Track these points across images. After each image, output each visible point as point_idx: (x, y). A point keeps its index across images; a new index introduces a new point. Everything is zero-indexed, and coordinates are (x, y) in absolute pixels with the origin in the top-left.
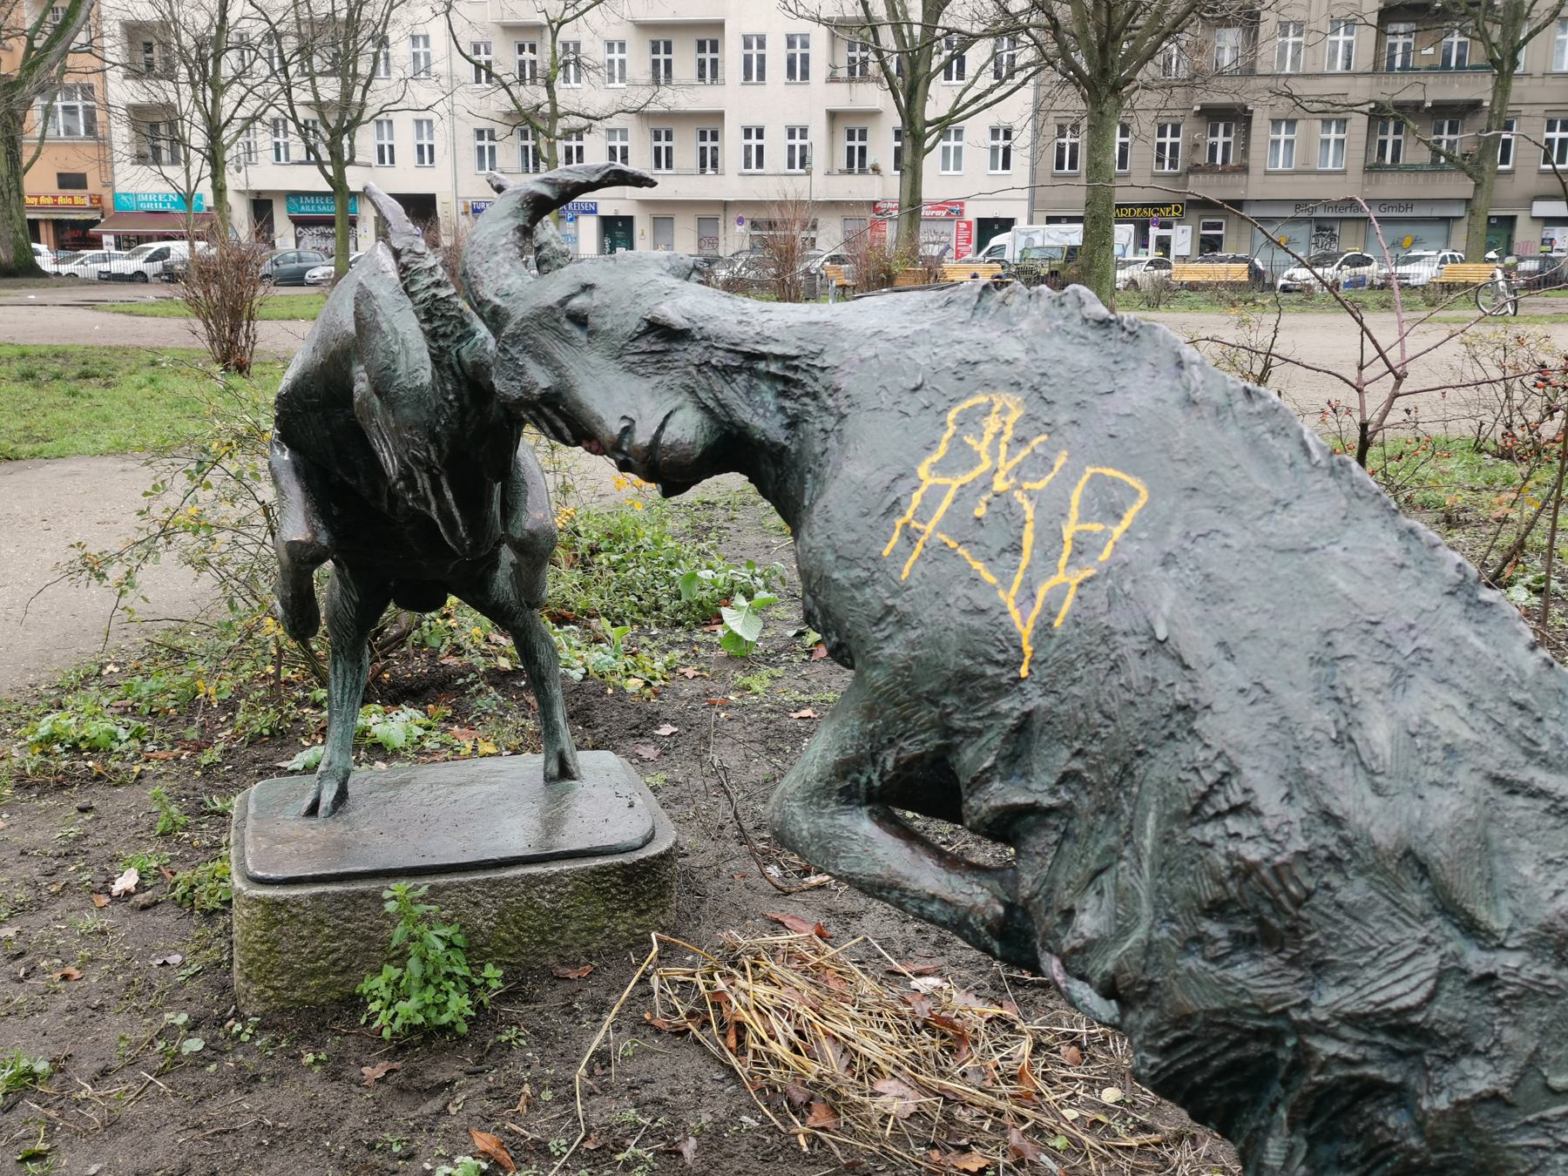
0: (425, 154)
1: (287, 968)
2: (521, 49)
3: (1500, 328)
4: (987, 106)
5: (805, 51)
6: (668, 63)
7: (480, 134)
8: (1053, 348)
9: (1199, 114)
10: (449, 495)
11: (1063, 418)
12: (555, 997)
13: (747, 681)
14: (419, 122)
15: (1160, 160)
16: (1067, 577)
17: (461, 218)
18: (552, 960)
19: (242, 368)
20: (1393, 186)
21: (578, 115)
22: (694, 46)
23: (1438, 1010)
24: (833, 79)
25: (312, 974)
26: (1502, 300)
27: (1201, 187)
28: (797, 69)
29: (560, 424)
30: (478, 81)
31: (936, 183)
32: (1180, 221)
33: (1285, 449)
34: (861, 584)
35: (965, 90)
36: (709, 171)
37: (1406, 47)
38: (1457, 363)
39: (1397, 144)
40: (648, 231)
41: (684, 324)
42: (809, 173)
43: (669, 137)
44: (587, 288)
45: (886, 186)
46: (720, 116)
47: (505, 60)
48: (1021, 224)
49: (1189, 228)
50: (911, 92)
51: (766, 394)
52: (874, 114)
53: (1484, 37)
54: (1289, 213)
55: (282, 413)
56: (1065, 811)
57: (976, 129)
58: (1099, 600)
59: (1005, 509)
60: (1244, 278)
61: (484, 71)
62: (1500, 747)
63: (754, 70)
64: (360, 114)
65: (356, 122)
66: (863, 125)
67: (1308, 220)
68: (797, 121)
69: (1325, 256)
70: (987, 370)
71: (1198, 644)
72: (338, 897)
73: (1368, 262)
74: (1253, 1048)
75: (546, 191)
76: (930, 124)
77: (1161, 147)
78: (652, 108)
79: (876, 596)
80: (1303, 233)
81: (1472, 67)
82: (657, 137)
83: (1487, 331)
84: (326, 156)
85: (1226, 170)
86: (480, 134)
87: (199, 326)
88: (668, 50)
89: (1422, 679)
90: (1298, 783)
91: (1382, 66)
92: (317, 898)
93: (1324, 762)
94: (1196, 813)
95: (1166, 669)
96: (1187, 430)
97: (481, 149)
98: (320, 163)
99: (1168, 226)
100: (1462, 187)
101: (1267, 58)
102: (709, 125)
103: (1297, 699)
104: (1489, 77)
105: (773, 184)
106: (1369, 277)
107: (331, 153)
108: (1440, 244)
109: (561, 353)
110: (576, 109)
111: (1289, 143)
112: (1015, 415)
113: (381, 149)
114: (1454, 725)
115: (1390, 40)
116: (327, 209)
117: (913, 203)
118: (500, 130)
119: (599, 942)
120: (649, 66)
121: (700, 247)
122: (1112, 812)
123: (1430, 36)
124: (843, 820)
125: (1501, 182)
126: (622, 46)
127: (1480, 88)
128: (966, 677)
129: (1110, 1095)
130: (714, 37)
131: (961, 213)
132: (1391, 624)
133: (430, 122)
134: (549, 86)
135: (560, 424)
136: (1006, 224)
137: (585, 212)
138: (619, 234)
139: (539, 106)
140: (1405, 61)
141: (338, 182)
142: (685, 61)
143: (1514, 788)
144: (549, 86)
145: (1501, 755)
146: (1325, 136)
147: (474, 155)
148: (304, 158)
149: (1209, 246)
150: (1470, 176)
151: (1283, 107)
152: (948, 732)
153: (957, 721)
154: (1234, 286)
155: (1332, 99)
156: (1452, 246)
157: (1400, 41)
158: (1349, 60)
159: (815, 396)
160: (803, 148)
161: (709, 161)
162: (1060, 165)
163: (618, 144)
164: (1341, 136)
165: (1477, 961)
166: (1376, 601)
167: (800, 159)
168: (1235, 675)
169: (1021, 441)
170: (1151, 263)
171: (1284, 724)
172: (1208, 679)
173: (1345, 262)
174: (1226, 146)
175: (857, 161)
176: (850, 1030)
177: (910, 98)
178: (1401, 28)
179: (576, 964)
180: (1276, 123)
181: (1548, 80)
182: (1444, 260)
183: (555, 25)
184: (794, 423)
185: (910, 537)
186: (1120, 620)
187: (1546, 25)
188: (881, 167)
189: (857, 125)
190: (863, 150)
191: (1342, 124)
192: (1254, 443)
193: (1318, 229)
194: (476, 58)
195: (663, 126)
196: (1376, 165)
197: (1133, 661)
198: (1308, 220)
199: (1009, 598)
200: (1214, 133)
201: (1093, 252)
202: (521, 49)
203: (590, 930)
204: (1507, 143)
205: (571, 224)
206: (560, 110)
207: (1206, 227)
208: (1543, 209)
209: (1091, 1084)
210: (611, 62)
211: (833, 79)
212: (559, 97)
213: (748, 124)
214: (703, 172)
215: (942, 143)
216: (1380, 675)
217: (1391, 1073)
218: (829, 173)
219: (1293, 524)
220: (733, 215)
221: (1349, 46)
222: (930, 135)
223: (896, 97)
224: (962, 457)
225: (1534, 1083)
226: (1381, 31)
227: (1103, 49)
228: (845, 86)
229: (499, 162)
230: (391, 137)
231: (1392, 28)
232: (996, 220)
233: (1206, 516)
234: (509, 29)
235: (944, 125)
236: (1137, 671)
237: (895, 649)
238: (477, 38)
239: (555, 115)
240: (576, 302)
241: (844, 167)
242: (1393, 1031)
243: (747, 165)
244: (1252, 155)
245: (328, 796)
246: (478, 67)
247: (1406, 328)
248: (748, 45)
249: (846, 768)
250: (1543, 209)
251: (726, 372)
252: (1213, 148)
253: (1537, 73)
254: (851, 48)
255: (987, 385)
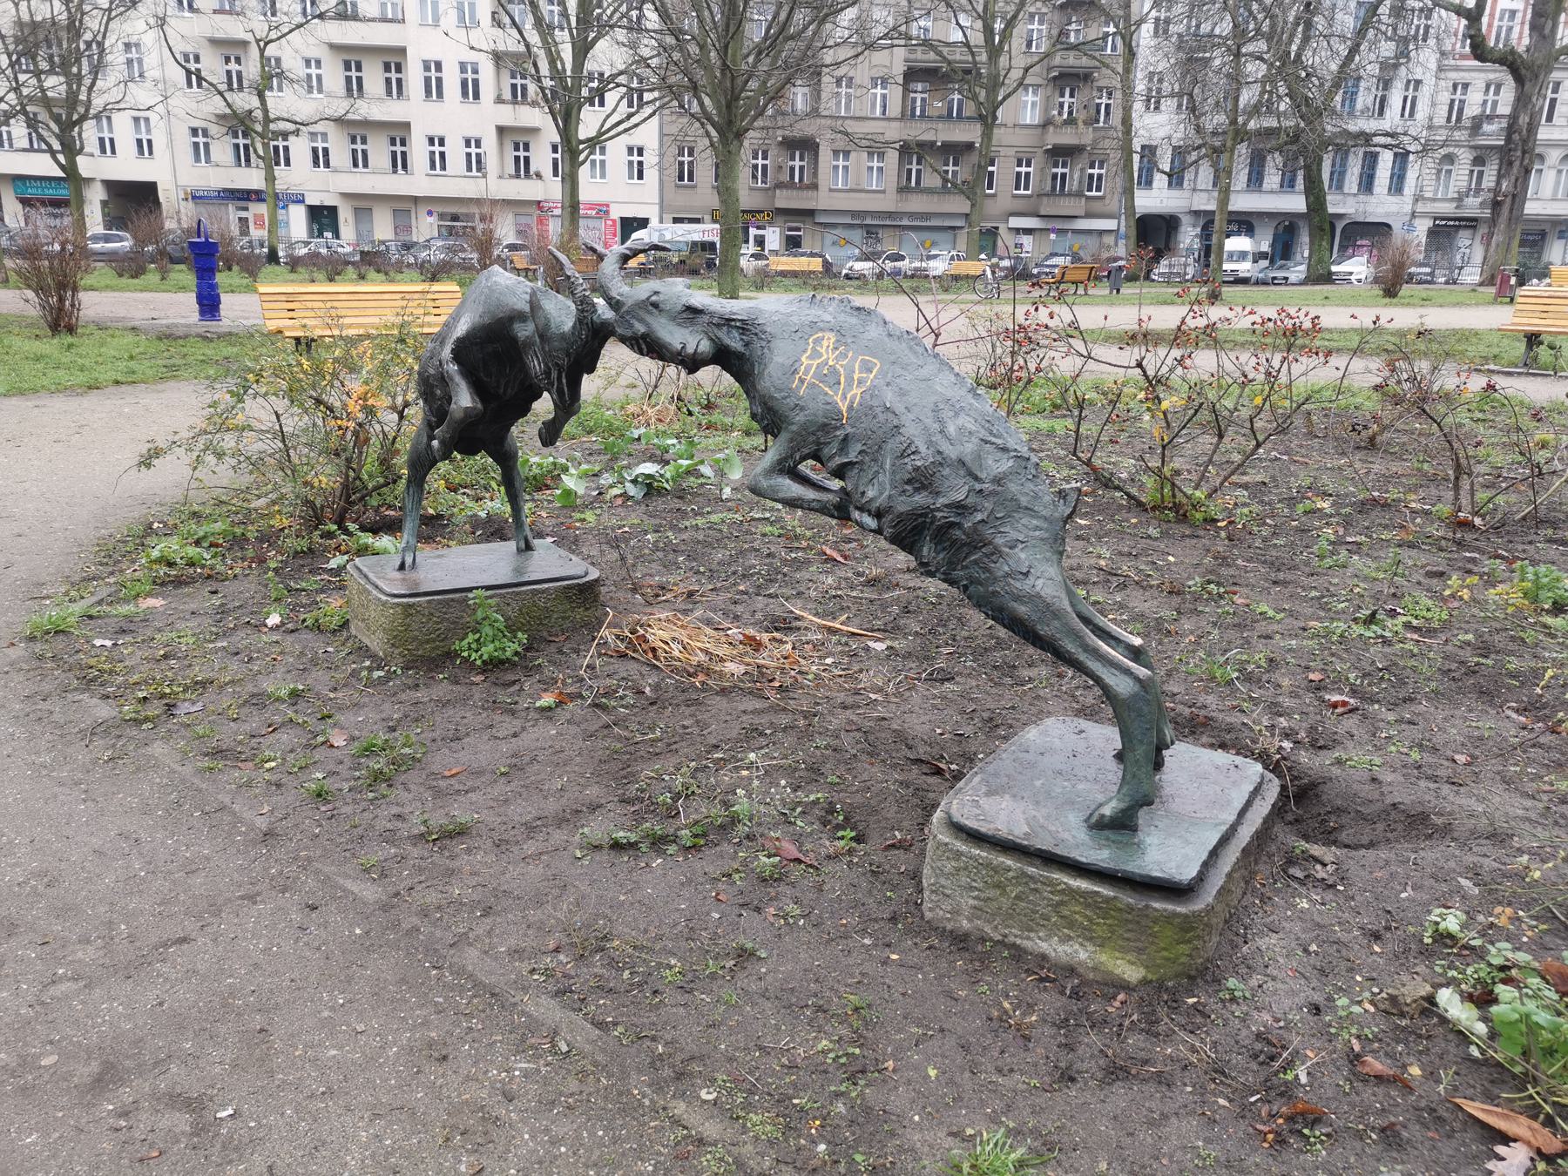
0: (144, 148)
1: (415, 639)
2: (227, 60)
3: (988, 308)
4: (626, 130)
5: (475, 76)
6: (359, 79)
7: (194, 131)
8: (842, 317)
9: (781, 143)
10: (564, 381)
11: (849, 341)
12: (553, 648)
13: (582, 516)
14: (136, 120)
15: (755, 177)
16: (856, 391)
17: (183, 203)
18: (545, 634)
19: (71, 330)
20: (917, 204)
21: (283, 119)
22: (381, 67)
23: (968, 500)
24: (499, 100)
25: (428, 642)
26: (990, 287)
27: (784, 200)
28: (470, 90)
29: (644, 346)
30: (190, 85)
31: (590, 189)
32: (771, 224)
33: (920, 350)
34: (785, 398)
35: (608, 116)
36: (400, 171)
37: (923, 100)
38: (964, 330)
39: (919, 172)
40: (351, 219)
41: (700, 307)
42: (485, 176)
43: (364, 141)
44: (656, 293)
45: (551, 189)
46: (406, 126)
47: (212, 67)
48: (654, 222)
49: (778, 230)
50: (567, 119)
51: (735, 333)
52: (534, 131)
53: (975, 97)
54: (848, 220)
55: (457, 346)
56: (861, 463)
57: (616, 151)
58: (868, 397)
59: (833, 371)
60: (820, 269)
61: (194, 77)
62: (983, 431)
63: (434, 89)
64: (87, 110)
65: (84, 118)
66: (525, 139)
67: (861, 226)
68: (473, 133)
69: (873, 253)
70: (821, 325)
71: (899, 408)
72: (440, 602)
73: (902, 258)
74: (920, 520)
75: (628, 252)
76: (582, 142)
77: (755, 167)
78: (350, 116)
79: (791, 402)
80: (857, 236)
81: (968, 118)
82: (354, 141)
83: (980, 309)
84: (56, 146)
85: (802, 187)
86: (194, 131)
87: (30, 294)
88: (359, 68)
89: (962, 415)
90: (930, 444)
91: (907, 115)
92: (429, 602)
93: (937, 438)
94: (902, 456)
95: (890, 415)
96: (891, 344)
97: (196, 145)
98: (53, 153)
99: (763, 228)
100: (960, 205)
101: (828, 106)
102: (398, 133)
103: (929, 422)
104: (979, 126)
105: (456, 184)
106: (903, 269)
107: (62, 144)
108: (949, 246)
109: (649, 319)
110: (285, 116)
111: (846, 168)
112: (833, 340)
113: (102, 140)
114: (971, 426)
115: (912, 95)
116: (63, 192)
117: (573, 206)
118: (214, 130)
119: (567, 624)
120: (343, 82)
121: (396, 234)
122: (875, 460)
123: (939, 94)
124: (780, 480)
125: (989, 202)
126: (318, 63)
127: (969, 133)
128: (825, 425)
129: (829, 661)
130: (397, 60)
131: (607, 212)
132: (954, 400)
133: (147, 120)
134: (261, 96)
135: (644, 346)
136: (643, 223)
137: (293, 202)
138: (325, 221)
139: (250, 112)
140: (923, 111)
141: (71, 171)
142: (373, 78)
143: (986, 442)
144: (261, 96)
145: (983, 434)
146: (870, 164)
147: (191, 150)
148: (27, 146)
149: (793, 243)
150: (968, 198)
151: (841, 143)
152: (819, 444)
153: (822, 440)
154: (810, 274)
155: (874, 137)
156: (958, 248)
157: (919, 96)
158: (885, 107)
159: (756, 334)
160: (478, 155)
161: (400, 162)
162: (681, 178)
163: (320, 145)
164: (881, 165)
165: (978, 487)
166: (949, 393)
167: (476, 164)
168: (911, 416)
169: (836, 348)
170: (752, 256)
171: (926, 429)
172: (903, 418)
173: (888, 258)
174: (801, 168)
175: (523, 168)
176: (708, 645)
177: (567, 120)
178: (920, 87)
179: (557, 636)
180: (836, 153)
181: (1017, 129)
182: (952, 258)
183: (262, 44)
184: (747, 345)
185: (802, 381)
186: (875, 403)
187: (1014, 91)
188: (543, 174)
189: (521, 139)
190: (527, 159)
191: (881, 156)
192: (911, 348)
193: (868, 233)
194: (188, 65)
195: (358, 132)
196: (906, 187)
197: (880, 415)
198: (861, 226)
199: (838, 399)
200: (793, 159)
201: (727, 251)
202: (227, 60)
203: (563, 618)
204: (991, 173)
205: (283, 211)
206: (272, 116)
207: (790, 229)
208: (1015, 222)
209: (820, 658)
210: (309, 76)
211: (499, 100)
212: (270, 103)
213: (431, 133)
214: (395, 172)
215: (592, 157)
216: (952, 413)
217: (957, 520)
218: (500, 177)
219: (924, 372)
220: (422, 211)
221: (884, 97)
222: (583, 151)
223: (555, 120)
224: (816, 354)
225: (992, 517)
226: (906, 90)
227: (729, 106)
228: (510, 107)
229: (213, 157)
230: (111, 130)
231: (912, 86)
232: (635, 219)
233: (899, 371)
234: (215, 42)
235: (596, 142)
236: (881, 417)
237: (800, 418)
238: (189, 49)
239: (267, 120)
240: (654, 298)
241: (513, 172)
242: (957, 508)
243: (433, 166)
244: (820, 176)
245: (409, 560)
246: (189, 72)
247: (940, 307)
248: (427, 68)
249: (780, 462)
250: (1015, 222)
251: (718, 326)
252: (792, 169)
253: (1010, 124)
254: (513, 77)
255: (822, 330)
